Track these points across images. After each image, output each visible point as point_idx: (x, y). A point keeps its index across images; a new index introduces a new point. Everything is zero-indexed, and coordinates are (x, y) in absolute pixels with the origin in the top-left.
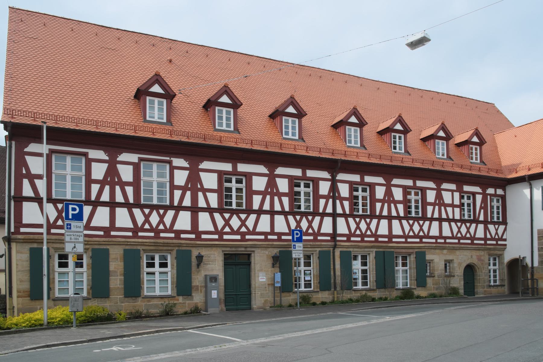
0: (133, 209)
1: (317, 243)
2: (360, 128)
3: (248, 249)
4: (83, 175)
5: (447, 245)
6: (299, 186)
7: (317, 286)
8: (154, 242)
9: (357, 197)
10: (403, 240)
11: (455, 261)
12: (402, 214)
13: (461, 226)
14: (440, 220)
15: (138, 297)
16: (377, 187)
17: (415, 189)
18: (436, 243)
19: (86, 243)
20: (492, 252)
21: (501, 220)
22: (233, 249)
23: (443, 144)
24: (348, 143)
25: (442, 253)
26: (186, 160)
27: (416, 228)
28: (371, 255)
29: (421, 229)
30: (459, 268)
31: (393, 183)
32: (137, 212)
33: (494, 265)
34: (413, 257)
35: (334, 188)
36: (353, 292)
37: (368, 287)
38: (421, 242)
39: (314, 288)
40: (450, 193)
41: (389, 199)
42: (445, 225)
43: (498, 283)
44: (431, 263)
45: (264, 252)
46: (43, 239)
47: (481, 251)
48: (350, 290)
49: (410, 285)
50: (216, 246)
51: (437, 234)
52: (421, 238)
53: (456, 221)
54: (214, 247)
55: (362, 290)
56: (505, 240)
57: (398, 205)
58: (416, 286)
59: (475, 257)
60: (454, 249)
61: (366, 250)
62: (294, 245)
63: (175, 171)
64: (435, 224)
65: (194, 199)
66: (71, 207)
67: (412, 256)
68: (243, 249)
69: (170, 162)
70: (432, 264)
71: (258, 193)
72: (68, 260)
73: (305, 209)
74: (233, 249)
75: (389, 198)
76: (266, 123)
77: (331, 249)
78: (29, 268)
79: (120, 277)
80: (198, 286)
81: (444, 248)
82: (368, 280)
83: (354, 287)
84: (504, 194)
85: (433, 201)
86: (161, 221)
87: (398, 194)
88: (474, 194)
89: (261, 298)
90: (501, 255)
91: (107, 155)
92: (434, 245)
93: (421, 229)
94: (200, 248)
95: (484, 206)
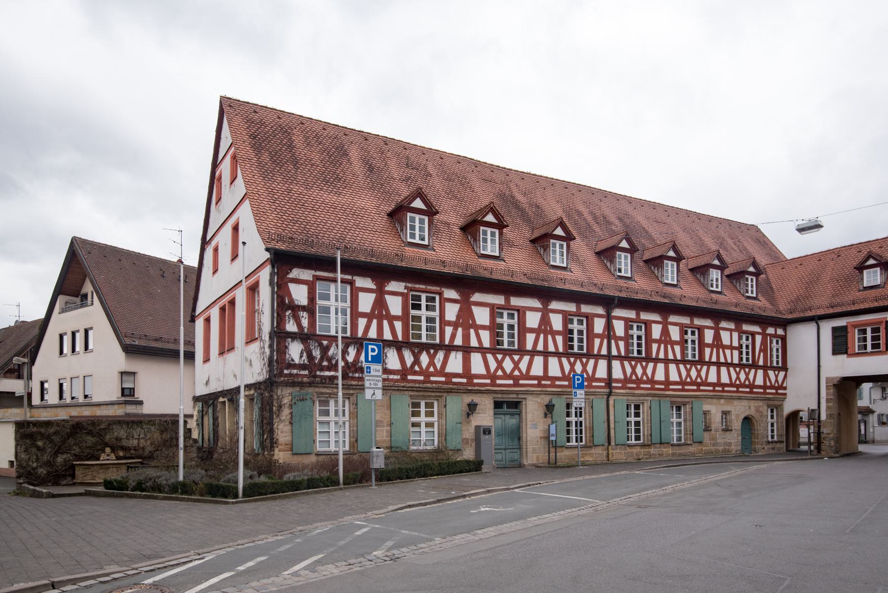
0: (624, 362)
2: (756, 276)
3: (520, 396)
4: (349, 307)
5: (725, 394)
6: (502, 317)
10: (680, 387)
12: (486, 343)
13: (740, 371)
14: (718, 364)
16: (654, 325)
17: (508, 309)
18: (714, 391)
19: (362, 387)
20: (770, 403)
21: (780, 365)
23: (672, 266)
24: (552, 261)
25: (720, 404)
26: (457, 291)
27: (694, 373)
28: (645, 405)
29: (699, 375)
30: (737, 421)
31: (614, 314)
35: (609, 327)
37: (642, 441)
39: (586, 442)
40: (728, 333)
41: (717, 343)
42: (724, 370)
44: (707, 415)
47: (759, 401)
49: (685, 440)
52: (698, 385)
55: (576, 447)
56: (785, 388)
57: (481, 332)
59: (753, 408)
60: (732, 398)
61: (641, 398)
62: (574, 392)
64: (713, 369)
65: (466, 337)
66: (370, 347)
67: (688, 406)
70: (709, 415)
71: (532, 330)
72: (420, 408)
73: (578, 350)
75: (545, 327)
76: (386, 224)
81: (721, 397)
82: (642, 434)
84: (784, 334)
87: (557, 322)
88: (753, 334)
89: (532, 453)
90: (782, 405)
91: (388, 284)
92: (712, 394)
93: (699, 375)
95: (764, 349)
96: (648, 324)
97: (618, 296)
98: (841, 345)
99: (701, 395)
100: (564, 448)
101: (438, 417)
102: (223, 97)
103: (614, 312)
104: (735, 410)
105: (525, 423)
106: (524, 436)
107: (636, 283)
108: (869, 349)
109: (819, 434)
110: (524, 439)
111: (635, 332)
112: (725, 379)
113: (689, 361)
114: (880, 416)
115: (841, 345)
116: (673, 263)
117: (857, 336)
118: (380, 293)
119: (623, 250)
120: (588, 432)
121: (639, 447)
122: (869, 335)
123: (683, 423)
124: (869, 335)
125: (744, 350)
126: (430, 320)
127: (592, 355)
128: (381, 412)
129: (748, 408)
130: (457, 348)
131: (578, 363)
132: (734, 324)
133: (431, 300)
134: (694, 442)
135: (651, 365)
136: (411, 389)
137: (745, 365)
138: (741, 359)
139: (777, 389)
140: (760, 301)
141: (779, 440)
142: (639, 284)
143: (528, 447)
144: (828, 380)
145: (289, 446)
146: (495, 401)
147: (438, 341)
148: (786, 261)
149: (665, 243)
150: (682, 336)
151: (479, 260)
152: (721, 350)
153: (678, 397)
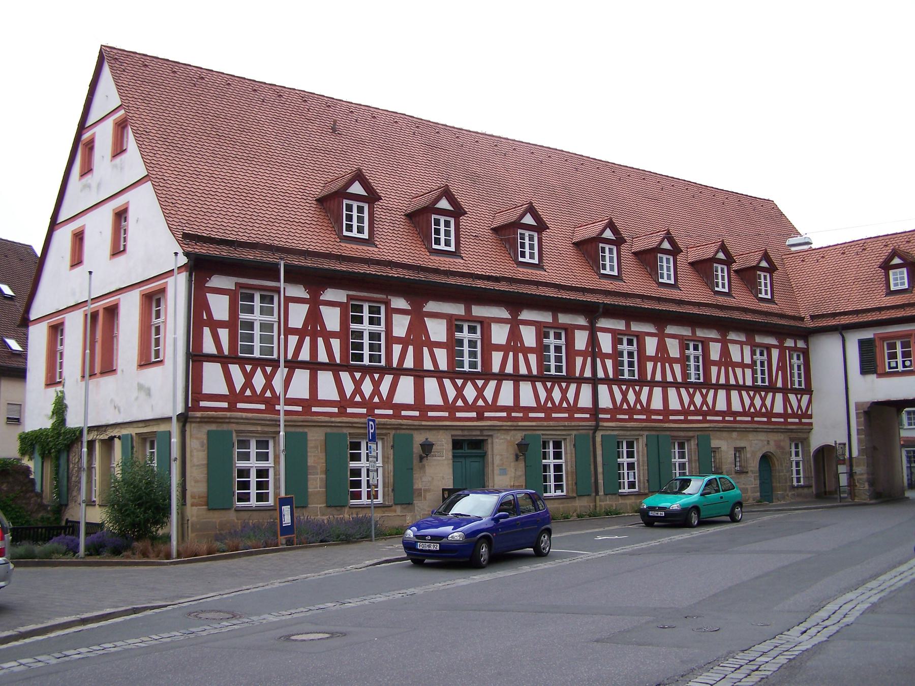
3: (486, 433)
5: (738, 425)
7: (573, 488)
8: (302, 420)
9: (460, 342)
10: (682, 418)
11: (748, 449)
12: (443, 366)
15: (344, 506)
18: (724, 421)
20: (794, 435)
21: (803, 386)
22: (466, 433)
27: (470, 393)
28: (640, 441)
30: (754, 461)
32: (235, 370)
33: (797, 454)
34: (693, 443)
35: (593, 341)
36: (620, 497)
37: (637, 489)
38: (705, 421)
40: (739, 346)
42: (734, 394)
43: (802, 483)
45: (506, 437)
47: (779, 434)
48: (615, 494)
51: (724, 408)
52: (704, 414)
53: (747, 388)
54: (441, 429)
57: (437, 351)
59: (772, 443)
60: (746, 431)
64: (722, 394)
65: (418, 358)
68: (478, 433)
69: (387, 304)
74: (466, 433)
75: (514, 344)
77: (591, 432)
78: (205, 462)
80: (421, 489)
83: (545, 495)
85: (504, 342)
86: (376, 391)
87: (529, 337)
88: (768, 348)
93: (705, 402)
95: (782, 367)
96: (485, 324)
97: (603, 303)
98: (869, 366)
101: (383, 462)
108: (900, 368)
112: (736, 406)
115: (869, 366)
117: (886, 351)
118: (515, 326)
119: (608, 241)
121: (633, 497)
122: (899, 350)
123: (687, 464)
124: (899, 350)
125: (759, 368)
128: (314, 456)
129: (766, 443)
130: (407, 372)
131: (757, 398)
133: (374, 310)
136: (350, 425)
139: (800, 417)
144: (858, 405)
150: (539, 339)
153: (681, 431)
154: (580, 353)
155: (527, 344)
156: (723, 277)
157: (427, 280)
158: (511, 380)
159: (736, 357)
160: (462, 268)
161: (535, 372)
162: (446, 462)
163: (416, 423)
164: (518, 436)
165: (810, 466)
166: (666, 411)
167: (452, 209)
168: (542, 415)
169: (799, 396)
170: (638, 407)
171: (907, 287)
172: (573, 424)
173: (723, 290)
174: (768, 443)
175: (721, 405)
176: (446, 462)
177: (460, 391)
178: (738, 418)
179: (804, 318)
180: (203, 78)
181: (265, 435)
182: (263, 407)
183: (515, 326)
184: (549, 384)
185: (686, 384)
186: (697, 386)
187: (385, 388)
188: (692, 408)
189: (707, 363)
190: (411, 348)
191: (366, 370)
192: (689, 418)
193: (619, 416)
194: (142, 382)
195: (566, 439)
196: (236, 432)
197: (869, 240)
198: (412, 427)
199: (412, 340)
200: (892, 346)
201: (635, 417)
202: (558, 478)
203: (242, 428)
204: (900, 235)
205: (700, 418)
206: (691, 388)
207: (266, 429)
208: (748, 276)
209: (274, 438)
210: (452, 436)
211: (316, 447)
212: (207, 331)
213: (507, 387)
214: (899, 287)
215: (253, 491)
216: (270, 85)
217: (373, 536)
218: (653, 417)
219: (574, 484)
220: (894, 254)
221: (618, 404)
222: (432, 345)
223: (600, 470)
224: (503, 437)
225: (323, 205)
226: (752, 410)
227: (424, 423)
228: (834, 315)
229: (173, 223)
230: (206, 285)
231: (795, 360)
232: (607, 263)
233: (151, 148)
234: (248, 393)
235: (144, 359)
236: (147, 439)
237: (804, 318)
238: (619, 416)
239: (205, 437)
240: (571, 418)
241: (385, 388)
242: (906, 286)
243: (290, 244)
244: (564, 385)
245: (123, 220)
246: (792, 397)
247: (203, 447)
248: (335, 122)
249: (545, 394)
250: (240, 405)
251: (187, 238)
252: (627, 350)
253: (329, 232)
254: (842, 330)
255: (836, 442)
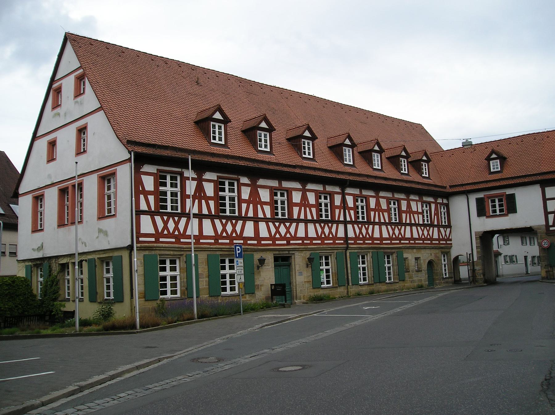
1: (336, 246)
3: (291, 252)
5: (416, 246)
10: (389, 242)
12: (268, 215)
15: (218, 296)
18: (409, 243)
19: (138, 248)
20: (443, 250)
21: (447, 224)
27: (283, 230)
28: (369, 255)
29: (288, 231)
30: (424, 264)
31: (205, 177)
35: (344, 201)
36: (360, 286)
37: (331, 285)
40: (415, 202)
42: (414, 228)
44: (406, 261)
46: (191, 248)
47: (436, 250)
50: (270, 250)
52: (400, 240)
54: (268, 251)
56: (451, 240)
58: (398, 280)
59: (433, 255)
63: (242, 187)
64: (408, 228)
65: (255, 211)
68: (287, 252)
69: (238, 181)
72: (225, 264)
75: (200, 193)
79: (205, 279)
84: (447, 202)
86: (234, 230)
88: (430, 203)
91: (204, 174)
94: (259, 252)
95: (436, 214)
96: (289, 191)
97: (349, 179)
98: (481, 212)
99: (402, 247)
100: (320, 289)
101: (180, 272)
102: (67, 33)
103: (411, 197)
104: (423, 257)
105: (294, 272)
106: (294, 281)
107: (357, 169)
108: (498, 213)
109: (474, 270)
110: (294, 284)
111: (359, 203)
112: (415, 235)
113: (360, 222)
114: (505, 257)
115: (481, 212)
116: (378, 154)
117: (490, 204)
118: (304, 192)
119: (347, 146)
120: (334, 276)
121: (366, 286)
122: (497, 203)
123: (391, 267)
124: (497, 203)
125: (425, 214)
126: (174, 194)
127: (293, 219)
128: (202, 268)
129: (430, 254)
130: (250, 219)
131: (396, 229)
132: (418, 196)
133: (231, 184)
134: (400, 281)
135: (371, 227)
136: (221, 250)
137: (426, 225)
138: (424, 220)
139: (446, 240)
140: (431, 180)
141: (450, 276)
142: (359, 169)
143: (297, 289)
144: (476, 233)
145: (143, 295)
146: (274, 257)
147: (237, 214)
148: (443, 151)
149: (372, 141)
150: (317, 200)
151: (258, 154)
152: (203, 202)
154: (337, 207)
155: (147, 188)
156: (349, 155)
157: (259, 167)
158: (303, 223)
159: (414, 209)
160: (275, 160)
161: (315, 218)
162: (271, 269)
163: (255, 247)
164: (308, 254)
165: (452, 267)
166: (381, 239)
167: (268, 128)
168: (320, 242)
169: (445, 229)
170: (368, 236)
171: (500, 170)
172: (336, 246)
173: (405, 172)
174: (431, 255)
175: (408, 235)
176: (271, 269)
177: (277, 229)
178: (416, 242)
179: (446, 187)
180: (124, 52)
181: (175, 257)
182: (174, 240)
183: (304, 192)
184: (322, 225)
185: (391, 224)
186: (396, 224)
187: (238, 228)
188: (394, 236)
189: (400, 212)
190: (251, 205)
191: (229, 218)
192: (393, 242)
193: (358, 242)
194: (101, 228)
195: (331, 255)
196: (159, 256)
197: (477, 145)
198: (253, 250)
199: (252, 201)
200: (493, 201)
201: (366, 242)
202: (174, 285)
203: (163, 252)
204: (493, 142)
205: (398, 242)
206: (367, 225)
207: (176, 253)
208: (416, 165)
209: (179, 258)
210: (274, 254)
211: (203, 263)
212: (142, 197)
213: (302, 226)
214: (496, 170)
215: (228, 286)
216: (161, 57)
217: (242, 312)
218: (375, 242)
219: (336, 280)
220: (493, 152)
221: (364, 236)
222: (263, 203)
223: (349, 271)
224: (300, 254)
225: (198, 125)
226: (423, 237)
227: (259, 247)
228: (462, 185)
229: (120, 134)
230: (141, 171)
231: (442, 210)
232: (307, 151)
233: (101, 91)
234: (166, 232)
235: (102, 214)
236: (106, 261)
237: (446, 187)
238: (358, 242)
239: (142, 258)
240: (334, 243)
241: (238, 228)
242: (499, 169)
243: (140, 140)
244: (330, 225)
245: (82, 134)
246: (442, 229)
247: (141, 264)
248: (198, 79)
249: (422, 233)
250: (161, 240)
251: (129, 143)
252: (324, 203)
253: (204, 140)
254: (467, 193)
255: (467, 253)
